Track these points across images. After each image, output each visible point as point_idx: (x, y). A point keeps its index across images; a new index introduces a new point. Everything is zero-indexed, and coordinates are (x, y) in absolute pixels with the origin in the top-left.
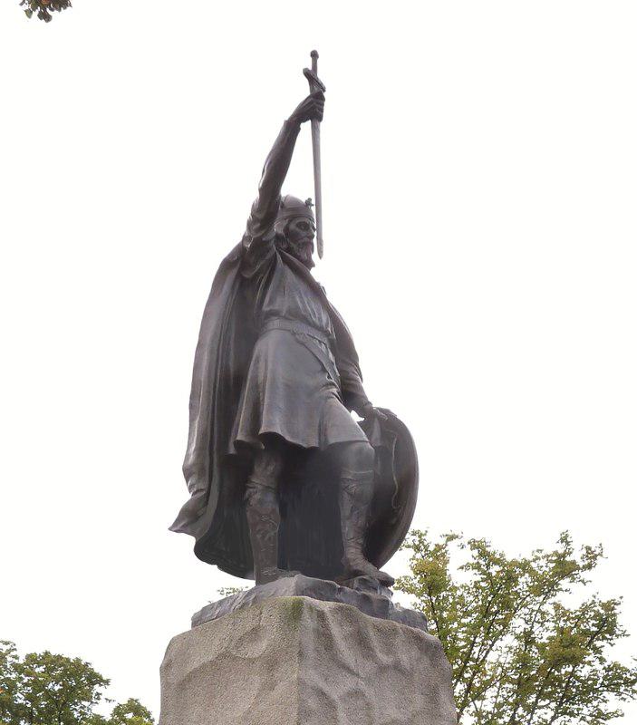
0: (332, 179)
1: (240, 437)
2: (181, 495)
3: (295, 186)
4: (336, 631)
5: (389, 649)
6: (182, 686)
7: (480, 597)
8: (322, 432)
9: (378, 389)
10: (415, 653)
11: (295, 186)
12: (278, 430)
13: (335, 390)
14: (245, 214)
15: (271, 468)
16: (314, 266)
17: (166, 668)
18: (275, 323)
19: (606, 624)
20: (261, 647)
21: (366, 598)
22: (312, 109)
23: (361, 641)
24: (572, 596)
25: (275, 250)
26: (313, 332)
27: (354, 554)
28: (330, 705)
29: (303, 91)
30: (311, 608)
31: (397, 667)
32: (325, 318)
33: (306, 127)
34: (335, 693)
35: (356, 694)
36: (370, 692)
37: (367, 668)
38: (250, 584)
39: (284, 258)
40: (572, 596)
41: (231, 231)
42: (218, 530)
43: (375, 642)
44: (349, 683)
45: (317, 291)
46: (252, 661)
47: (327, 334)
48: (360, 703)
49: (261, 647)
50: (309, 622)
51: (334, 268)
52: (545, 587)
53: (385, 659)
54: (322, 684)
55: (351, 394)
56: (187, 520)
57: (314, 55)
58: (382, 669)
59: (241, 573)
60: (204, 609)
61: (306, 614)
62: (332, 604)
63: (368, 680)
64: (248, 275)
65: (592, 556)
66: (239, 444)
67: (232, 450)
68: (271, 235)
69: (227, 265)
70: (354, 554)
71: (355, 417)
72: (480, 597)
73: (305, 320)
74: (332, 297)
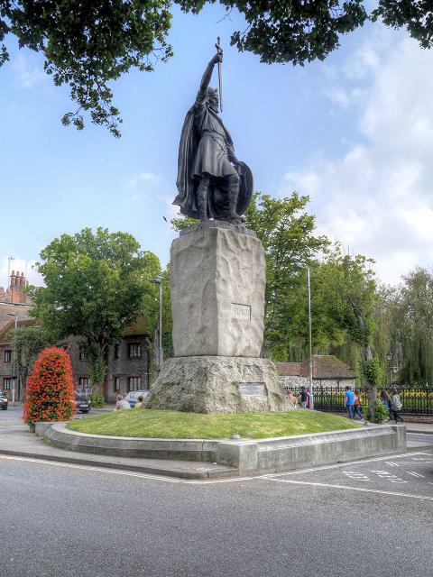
1: (195, 173)
2: (176, 193)
3: (213, 85)
4: (228, 238)
6: (178, 256)
9: (239, 157)
11: (213, 160)
14: (195, 94)
16: (264, 60)
17: (172, 250)
19: (309, 226)
20: (204, 244)
22: (217, 60)
23: (236, 241)
24: (298, 214)
27: (234, 211)
29: (215, 52)
31: (247, 250)
32: (223, 131)
33: (216, 65)
36: (238, 258)
40: (298, 214)
41: (190, 101)
46: (201, 248)
49: (204, 244)
52: (290, 211)
57: (218, 39)
58: (243, 250)
61: (219, 234)
63: (238, 254)
65: (306, 199)
66: (195, 175)
67: (192, 177)
69: (189, 113)
70: (234, 211)
71: (232, 164)
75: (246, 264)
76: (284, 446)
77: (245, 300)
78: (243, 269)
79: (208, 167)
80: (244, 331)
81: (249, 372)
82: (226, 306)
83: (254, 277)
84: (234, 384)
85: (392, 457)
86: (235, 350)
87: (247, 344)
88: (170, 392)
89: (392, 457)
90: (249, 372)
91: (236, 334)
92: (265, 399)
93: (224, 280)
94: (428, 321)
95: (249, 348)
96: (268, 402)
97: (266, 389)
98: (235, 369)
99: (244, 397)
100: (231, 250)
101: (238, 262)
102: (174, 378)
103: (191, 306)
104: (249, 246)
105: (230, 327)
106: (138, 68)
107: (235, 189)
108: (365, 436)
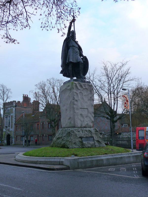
0: (78, 28)
2: (61, 69)
3: (72, 29)
5: (85, 86)
7: (126, 136)
8: (77, 60)
9: (84, 54)
10: (88, 87)
12: (71, 61)
13: (79, 55)
15: (71, 65)
18: (71, 47)
21: (82, 81)
23: (81, 86)
25: (71, 36)
26: (76, 48)
27: (82, 75)
28: (77, 94)
30: (74, 83)
31: (86, 89)
32: (77, 46)
34: (78, 92)
35: (81, 92)
36: (82, 92)
37: (81, 89)
38: (69, 79)
39: (72, 39)
42: (65, 72)
43: (83, 86)
44: (80, 91)
45: (76, 43)
47: (77, 48)
48: (81, 93)
50: (74, 85)
51: (78, 38)
53: (84, 88)
54: (76, 92)
55: (81, 55)
56: (62, 72)
58: (84, 89)
59: (68, 76)
60: (80, 49)
62: (77, 82)
63: (82, 90)
64: (68, 41)
67: (67, 63)
68: (70, 36)
70: (82, 75)
72: (126, 136)
73: (74, 46)
74: (79, 43)
75: (86, 94)
76: (90, 159)
77: (86, 107)
78: (84, 96)
79: (71, 60)
80: (85, 118)
81: (87, 133)
82: (77, 109)
83: (89, 98)
84: (80, 137)
85: (85, 157)
86: (82, 125)
87: (86, 123)
88: (58, 141)
89: (85, 157)
90: (87, 133)
91: (82, 120)
92: (93, 143)
93: (76, 100)
94: (147, 106)
95: (87, 124)
96: (94, 144)
97: (94, 139)
98: (81, 132)
99: (84, 142)
100: (79, 89)
101: (82, 93)
102: (60, 136)
103: (66, 110)
104: (87, 87)
105: (80, 117)
106: (29, 6)
107: (81, 67)
108: (128, 156)
